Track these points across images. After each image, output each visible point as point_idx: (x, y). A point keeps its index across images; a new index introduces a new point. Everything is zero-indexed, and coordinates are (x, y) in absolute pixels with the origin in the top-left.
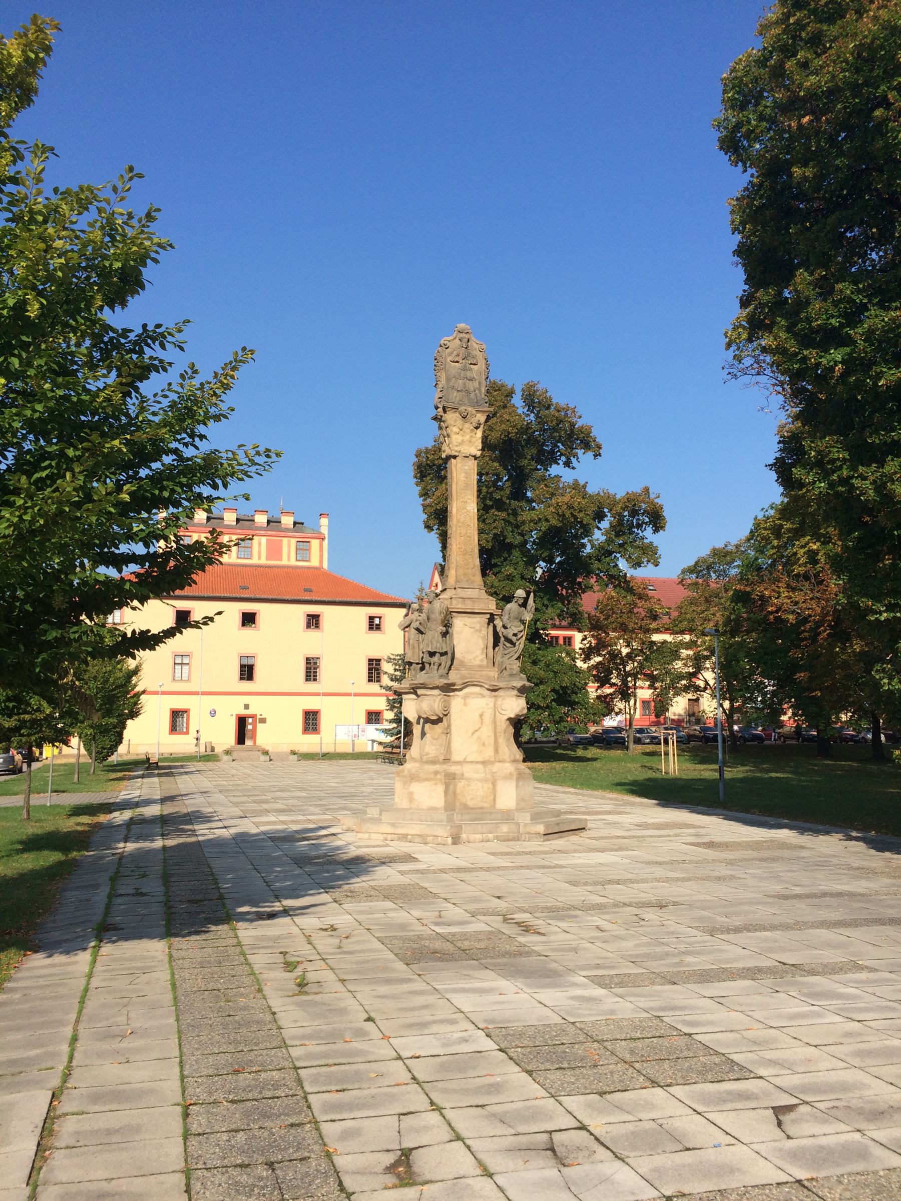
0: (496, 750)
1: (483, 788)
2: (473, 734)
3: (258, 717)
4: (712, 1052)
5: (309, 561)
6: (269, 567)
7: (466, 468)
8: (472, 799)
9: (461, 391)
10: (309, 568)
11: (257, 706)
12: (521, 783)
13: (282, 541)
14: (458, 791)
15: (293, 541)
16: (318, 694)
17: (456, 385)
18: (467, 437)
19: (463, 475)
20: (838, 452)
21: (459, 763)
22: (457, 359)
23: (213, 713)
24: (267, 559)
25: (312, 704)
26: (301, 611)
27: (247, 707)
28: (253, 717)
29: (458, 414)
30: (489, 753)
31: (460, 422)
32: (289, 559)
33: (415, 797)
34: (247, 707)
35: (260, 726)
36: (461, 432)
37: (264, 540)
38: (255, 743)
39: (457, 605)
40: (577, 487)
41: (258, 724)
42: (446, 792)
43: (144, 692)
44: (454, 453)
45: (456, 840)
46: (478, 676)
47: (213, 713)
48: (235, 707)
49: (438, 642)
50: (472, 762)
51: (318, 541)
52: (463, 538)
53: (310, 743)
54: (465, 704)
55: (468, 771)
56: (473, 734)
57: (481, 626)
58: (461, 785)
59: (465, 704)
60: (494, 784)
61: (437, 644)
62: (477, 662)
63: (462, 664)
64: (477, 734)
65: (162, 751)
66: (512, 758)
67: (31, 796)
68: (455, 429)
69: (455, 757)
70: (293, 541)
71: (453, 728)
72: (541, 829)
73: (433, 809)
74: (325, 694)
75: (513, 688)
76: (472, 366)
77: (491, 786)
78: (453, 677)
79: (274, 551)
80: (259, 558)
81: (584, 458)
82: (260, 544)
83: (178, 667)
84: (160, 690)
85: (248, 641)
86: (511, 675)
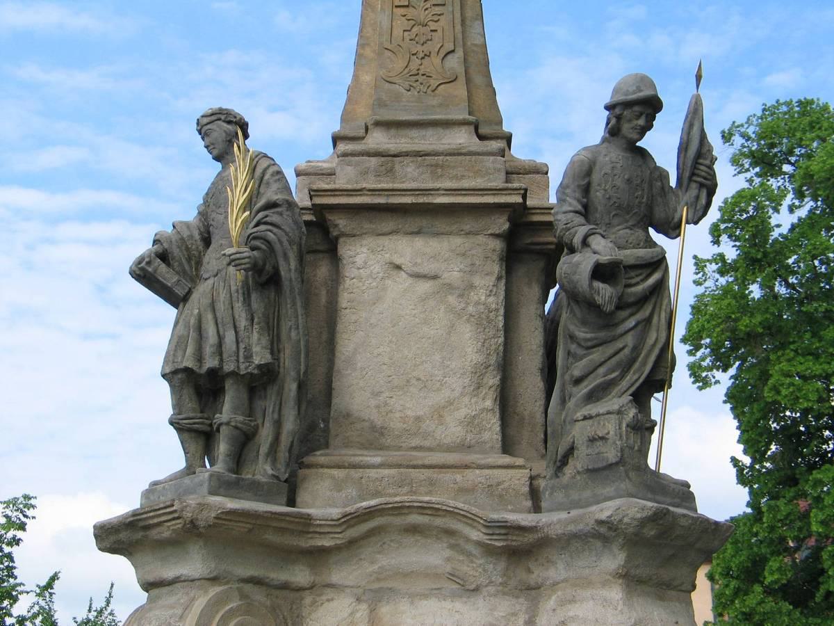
57: (472, 270)
62: (452, 431)
63: (375, 438)
75: (605, 534)
86: (597, 472)
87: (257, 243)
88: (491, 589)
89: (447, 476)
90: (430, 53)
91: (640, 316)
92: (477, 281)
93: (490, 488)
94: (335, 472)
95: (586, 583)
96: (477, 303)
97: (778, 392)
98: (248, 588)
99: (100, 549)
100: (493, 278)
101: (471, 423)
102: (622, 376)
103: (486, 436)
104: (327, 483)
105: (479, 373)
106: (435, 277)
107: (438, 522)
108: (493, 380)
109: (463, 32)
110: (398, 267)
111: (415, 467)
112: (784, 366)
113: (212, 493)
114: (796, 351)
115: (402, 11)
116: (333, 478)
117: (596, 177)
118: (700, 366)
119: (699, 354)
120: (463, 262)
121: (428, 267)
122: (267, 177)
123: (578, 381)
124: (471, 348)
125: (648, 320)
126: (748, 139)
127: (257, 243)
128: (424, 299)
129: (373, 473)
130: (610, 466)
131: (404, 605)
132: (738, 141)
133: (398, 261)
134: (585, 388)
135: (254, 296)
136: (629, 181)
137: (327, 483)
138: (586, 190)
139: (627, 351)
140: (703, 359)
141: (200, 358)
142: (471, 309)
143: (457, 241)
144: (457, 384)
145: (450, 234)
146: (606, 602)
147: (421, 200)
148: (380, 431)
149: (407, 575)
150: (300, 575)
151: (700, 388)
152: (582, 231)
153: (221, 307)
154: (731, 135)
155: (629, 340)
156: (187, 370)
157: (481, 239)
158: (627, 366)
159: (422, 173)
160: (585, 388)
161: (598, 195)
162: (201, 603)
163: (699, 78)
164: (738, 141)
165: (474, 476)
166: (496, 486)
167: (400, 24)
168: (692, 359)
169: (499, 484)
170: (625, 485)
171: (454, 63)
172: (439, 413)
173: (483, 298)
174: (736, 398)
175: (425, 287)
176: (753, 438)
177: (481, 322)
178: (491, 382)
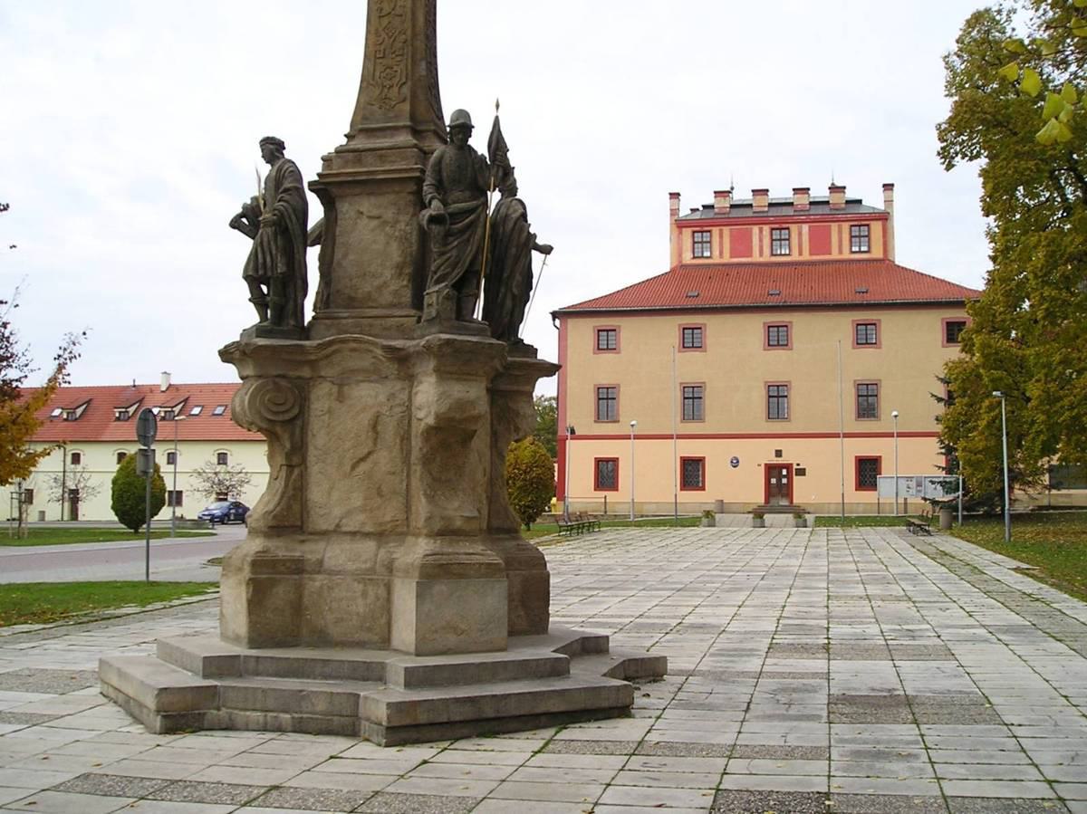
2: (354, 467)
3: (795, 467)
4: (150, 797)
10: (709, 266)
11: (794, 452)
13: (751, 229)
20: (962, 80)
23: (735, 463)
24: (811, 254)
25: (693, 449)
26: (846, 321)
27: (779, 453)
28: (788, 467)
32: (761, 254)
34: (779, 453)
35: (796, 479)
37: (805, 228)
38: (792, 502)
41: (795, 478)
47: (735, 463)
48: (764, 452)
50: (353, 534)
51: (880, 223)
53: (693, 500)
55: (337, 554)
56: (354, 467)
62: (387, 297)
64: (363, 467)
67: (151, 541)
77: (382, 591)
80: (800, 254)
82: (800, 234)
87: (276, 212)
88: (393, 376)
89: (378, 322)
90: (32, 360)
91: (465, 237)
92: (401, 218)
94: (327, 321)
96: (400, 230)
98: (277, 380)
99: (223, 361)
100: (409, 216)
102: (453, 270)
103: (403, 299)
104: (323, 327)
105: (400, 267)
106: (379, 218)
107: (363, 346)
109: (413, 69)
110: (362, 213)
111: (363, 318)
113: (257, 336)
115: (381, 60)
116: (325, 324)
117: (443, 165)
121: (375, 212)
122: (286, 174)
125: (468, 240)
127: (276, 212)
129: (344, 321)
130: (434, 318)
133: (361, 210)
135: (279, 237)
136: (459, 167)
137: (323, 327)
139: (452, 258)
142: (397, 234)
143: (392, 197)
145: (388, 193)
147: (371, 177)
148: (351, 299)
149: (353, 371)
150: (306, 372)
153: (265, 244)
155: (454, 253)
157: (404, 195)
158: (454, 266)
159: (18, 380)
163: (498, 106)
167: (379, 69)
169: (402, 325)
172: (380, 288)
173: (403, 227)
175: (375, 222)
178: (407, 271)
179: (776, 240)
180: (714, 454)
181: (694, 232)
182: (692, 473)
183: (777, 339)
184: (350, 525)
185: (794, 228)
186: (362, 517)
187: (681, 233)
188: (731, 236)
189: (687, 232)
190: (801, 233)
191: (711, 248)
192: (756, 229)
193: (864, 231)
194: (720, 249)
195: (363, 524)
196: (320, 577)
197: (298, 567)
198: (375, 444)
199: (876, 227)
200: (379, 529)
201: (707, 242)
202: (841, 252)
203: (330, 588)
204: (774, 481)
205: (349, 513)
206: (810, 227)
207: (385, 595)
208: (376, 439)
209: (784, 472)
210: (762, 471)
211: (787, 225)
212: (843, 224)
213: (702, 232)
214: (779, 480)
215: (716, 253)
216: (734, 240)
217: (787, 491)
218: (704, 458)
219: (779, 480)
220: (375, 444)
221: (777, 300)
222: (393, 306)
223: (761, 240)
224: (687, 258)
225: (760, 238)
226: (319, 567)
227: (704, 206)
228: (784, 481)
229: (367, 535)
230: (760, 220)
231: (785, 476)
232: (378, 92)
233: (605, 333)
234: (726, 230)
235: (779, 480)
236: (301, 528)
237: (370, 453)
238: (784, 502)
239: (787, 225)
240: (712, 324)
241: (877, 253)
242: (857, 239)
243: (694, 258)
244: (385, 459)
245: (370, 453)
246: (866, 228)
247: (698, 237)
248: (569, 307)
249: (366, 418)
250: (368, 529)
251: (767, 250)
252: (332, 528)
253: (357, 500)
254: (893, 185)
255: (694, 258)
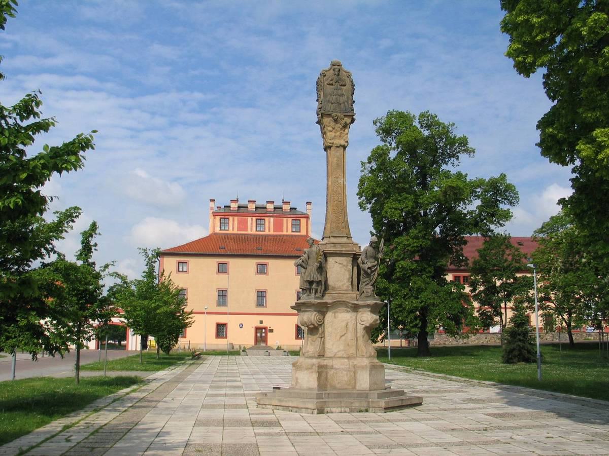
0: (357, 349)
1: (347, 375)
3: (268, 328)
5: (300, 232)
6: (292, 236)
7: (338, 154)
8: (339, 383)
9: (334, 103)
11: (268, 322)
12: (373, 372)
14: (329, 377)
15: (290, 220)
16: (226, 314)
17: (331, 100)
18: (338, 134)
19: (336, 159)
21: (331, 358)
22: (331, 82)
23: (241, 326)
24: (274, 232)
25: (222, 319)
27: (261, 322)
28: (265, 328)
29: (331, 118)
30: (352, 351)
31: (332, 124)
32: (251, 230)
33: (299, 381)
34: (261, 322)
35: (269, 334)
36: (334, 131)
37: (272, 219)
38: (267, 344)
39: (330, 248)
40: (459, 176)
42: (319, 378)
43: (191, 313)
44: (329, 144)
45: (321, 411)
46: (345, 298)
47: (241, 326)
48: (255, 321)
49: (314, 273)
50: (339, 357)
51: (305, 219)
52: (335, 203)
53: (222, 344)
54: (335, 317)
55: (337, 363)
57: (348, 263)
58: (331, 372)
59: (335, 317)
60: (355, 373)
61: (317, 277)
62: (345, 288)
63: (334, 289)
64: (343, 338)
65: (207, 348)
66: (368, 355)
68: (330, 129)
69: (328, 354)
70: (290, 220)
71: (326, 334)
72: (382, 403)
73: (310, 389)
74: (230, 314)
75: (368, 306)
76: (342, 87)
77: (352, 374)
78: (328, 299)
79: (278, 226)
80: (269, 231)
81: (463, 156)
82: (269, 222)
83: (260, 298)
84: (206, 311)
85: (261, 282)
86: (367, 297)
89: (344, 295)
93: (351, 297)
95: (365, 311)
97: (387, 213)
101: (348, 287)
105: (349, 279)
108: (351, 280)
112: (389, 205)
114: (393, 200)
118: (362, 203)
119: (362, 199)
120: (347, 261)
123: (364, 282)
124: (347, 275)
126: (382, 124)
128: (341, 267)
131: (339, 314)
132: (378, 124)
134: (365, 284)
138: (366, 254)
140: (363, 201)
141: (310, 278)
143: (346, 258)
144: (345, 281)
146: (368, 314)
151: (362, 211)
152: (366, 261)
154: (376, 122)
156: (308, 280)
160: (365, 284)
161: (368, 254)
162: (313, 315)
164: (378, 124)
165: (349, 295)
166: (352, 297)
168: (360, 200)
170: (372, 299)
171: (343, 224)
172: (343, 285)
174: (373, 212)
175: (341, 265)
176: (377, 224)
177: (349, 271)
179: (258, 224)
180: (232, 323)
181: (221, 218)
182: (221, 330)
183: (262, 270)
184: (340, 354)
185: (231, 218)
186: (343, 353)
187: (215, 218)
188: (238, 220)
189: (218, 218)
190: (270, 222)
191: (228, 226)
192: (249, 219)
193: (262, 222)
194: (233, 227)
195: (343, 355)
196: (333, 370)
197: (326, 367)
198: (347, 331)
199: (303, 221)
200: (348, 356)
201: (258, 224)
202: (287, 231)
203: (336, 373)
204: (259, 335)
205: (339, 351)
206: (274, 219)
207: (353, 375)
208: (347, 330)
209: (264, 331)
210: (253, 330)
211: (264, 218)
212: (253, 218)
213: (225, 218)
214: (261, 334)
215: (231, 228)
216: (239, 223)
217: (264, 339)
218: (227, 324)
219: (261, 334)
220: (347, 331)
221: (260, 250)
222: (346, 290)
223: (252, 224)
224: (218, 230)
225: (251, 222)
226: (332, 367)
227: (225, 207)
228: (264, 335)
229: (344, 357)
230: (252, 215)
231: (264, 333)
232: (335, 225)
233: (182, 264)
234: (236, 218)
235: (261, 334)
236: (323, 356)
237: (345, 334)
238: (263, 345)
239: (264, 218)
240: (271, 263)
241: (303, 233)
242: (295, 226)
243: (221, 230)
244: (350, 335)
245: (345, 334)
246: (299, 221)
247: (223, 220)
248: (165, 250)
249: (344, 324)
250: (344, 356)
251: (254, 229)
252: (332, 355)
253: (342, 348)
254: (311, 203)
255: (221, 230)
